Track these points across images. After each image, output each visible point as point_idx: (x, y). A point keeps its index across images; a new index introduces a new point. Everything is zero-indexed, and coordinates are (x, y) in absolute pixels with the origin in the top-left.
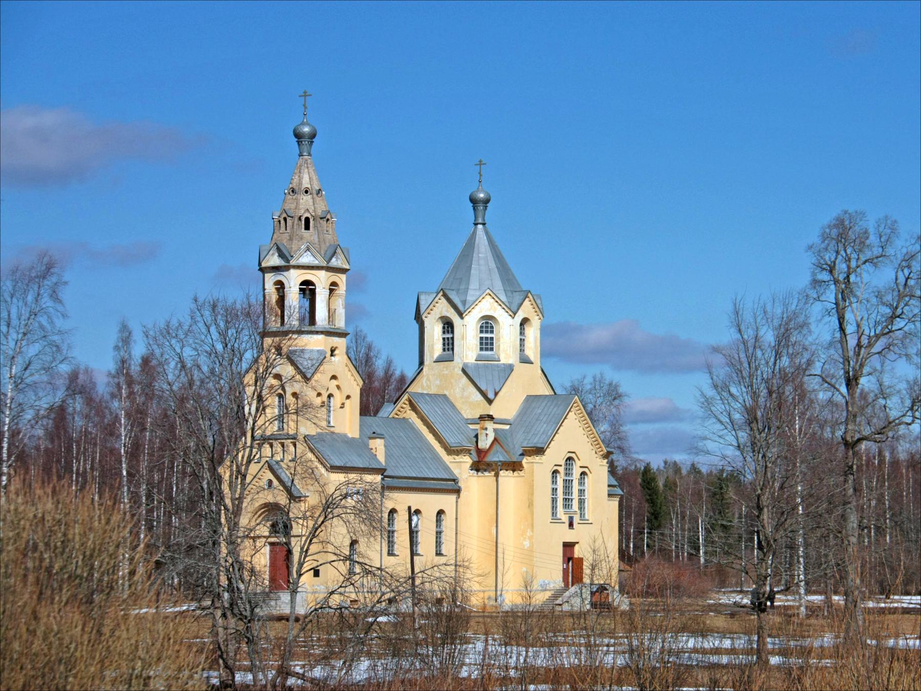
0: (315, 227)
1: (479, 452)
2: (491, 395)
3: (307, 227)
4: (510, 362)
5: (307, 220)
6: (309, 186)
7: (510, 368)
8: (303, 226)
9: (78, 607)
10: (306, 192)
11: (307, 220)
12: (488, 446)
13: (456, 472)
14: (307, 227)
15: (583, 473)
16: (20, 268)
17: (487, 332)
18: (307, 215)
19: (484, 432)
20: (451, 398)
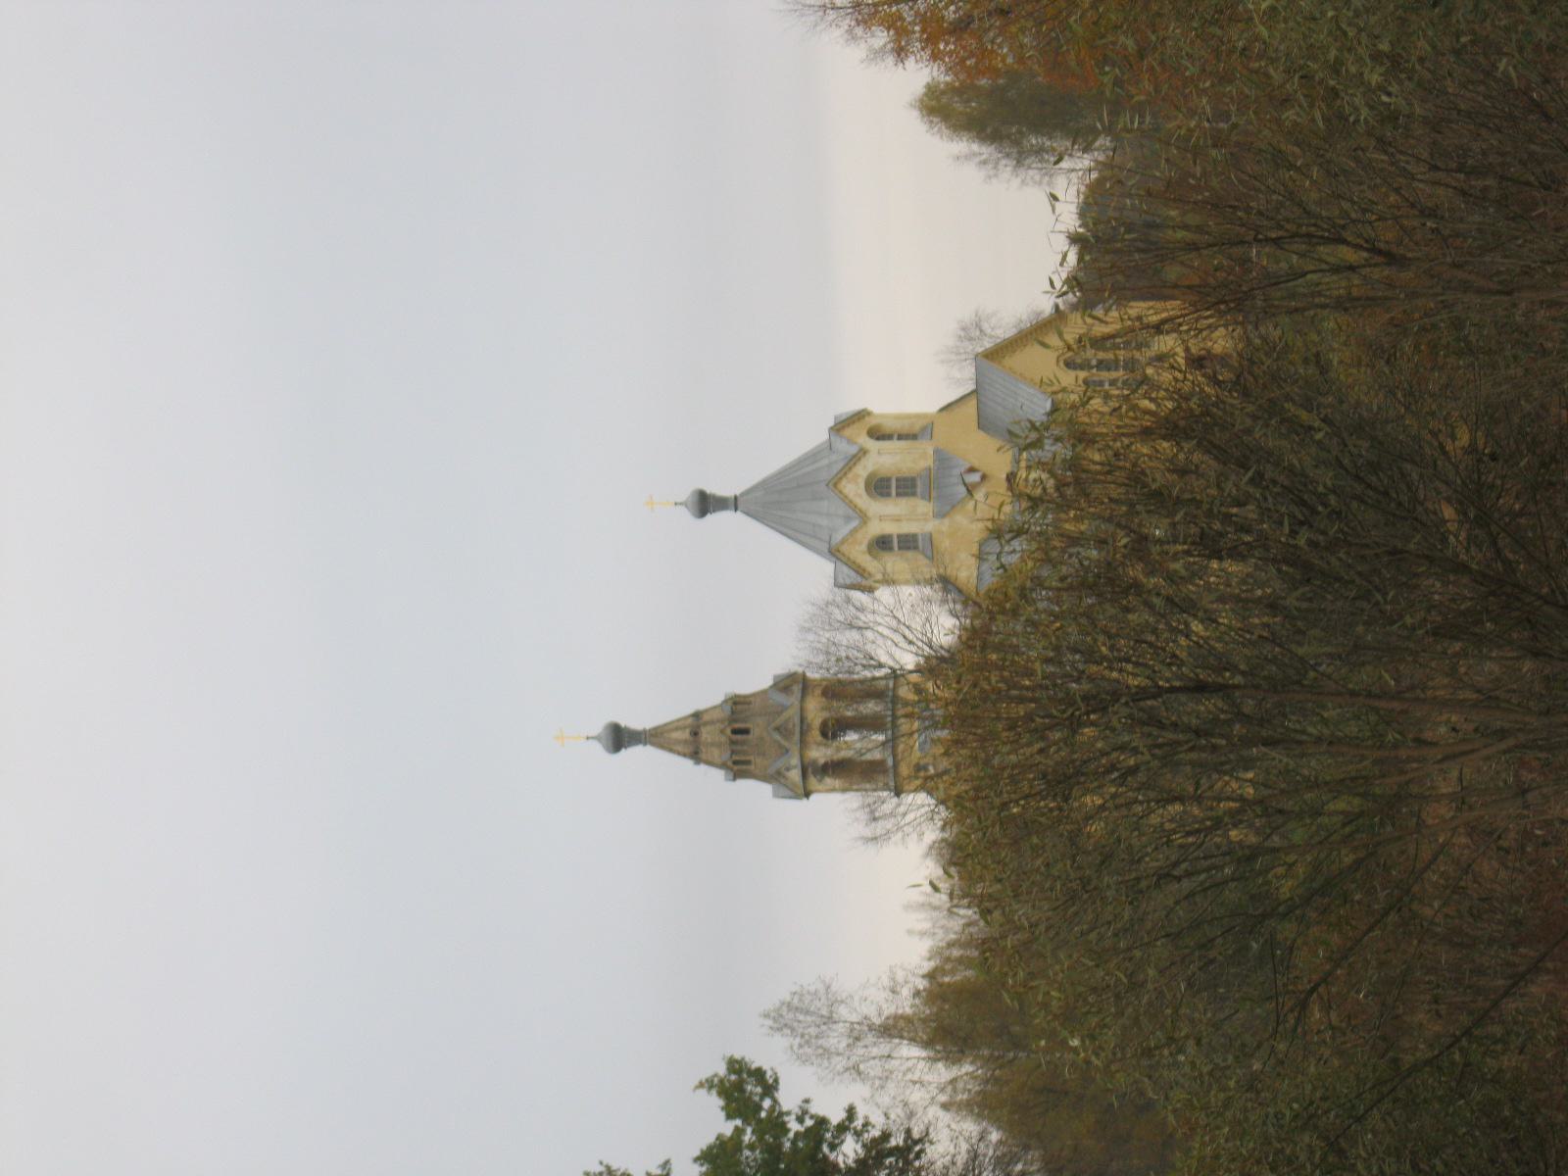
3: (746, 731)
4: (931, 452)
5: (735, 732)
7: (937, 452)
11: (735, 732)
14: (746, 731)
17: (889, 487)
18: (728, 731)
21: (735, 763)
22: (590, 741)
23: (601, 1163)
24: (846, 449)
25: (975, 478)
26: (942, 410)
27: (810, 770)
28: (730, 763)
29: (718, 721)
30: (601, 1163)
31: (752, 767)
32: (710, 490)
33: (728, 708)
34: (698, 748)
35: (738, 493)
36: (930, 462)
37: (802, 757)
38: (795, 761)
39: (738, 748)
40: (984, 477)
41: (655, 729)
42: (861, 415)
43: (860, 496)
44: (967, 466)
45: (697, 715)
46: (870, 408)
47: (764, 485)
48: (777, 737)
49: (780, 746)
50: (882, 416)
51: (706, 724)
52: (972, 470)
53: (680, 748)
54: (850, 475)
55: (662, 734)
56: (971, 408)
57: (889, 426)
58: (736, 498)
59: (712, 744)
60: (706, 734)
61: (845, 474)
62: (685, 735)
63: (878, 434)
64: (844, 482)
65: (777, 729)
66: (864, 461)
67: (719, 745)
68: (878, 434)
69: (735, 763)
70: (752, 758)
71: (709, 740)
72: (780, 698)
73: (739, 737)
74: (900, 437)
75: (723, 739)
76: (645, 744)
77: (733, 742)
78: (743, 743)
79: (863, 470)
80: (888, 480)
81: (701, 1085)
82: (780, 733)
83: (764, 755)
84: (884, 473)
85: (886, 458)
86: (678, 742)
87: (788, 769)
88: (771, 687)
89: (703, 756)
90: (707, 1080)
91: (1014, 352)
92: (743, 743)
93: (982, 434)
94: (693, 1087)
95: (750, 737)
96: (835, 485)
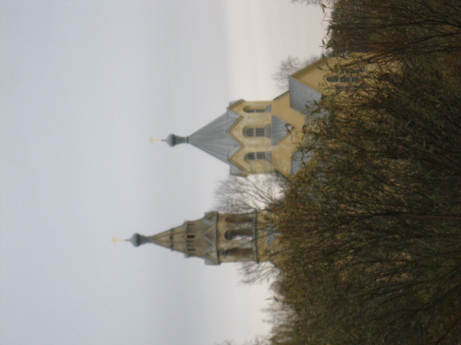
3: (193, 237)
4: (270, 117)
14: (193, 237)
18: (186, 237)
38: (214, 249)
40: (293, 128)
42: (240, 102)
45: (172, 230)
48: (206, 239)
51: (176, 234)
54: (236, 128)
56: (287, 99)
57: (253, 107)
60: (177, 238)
61: (234, 127)
62: (167, 238)
64: (234, 130)
65: (206, 235)
69: (189, 250)
73: (190, 239)
77: (188, 241)
79: (241, 125)
95: (195, 239)
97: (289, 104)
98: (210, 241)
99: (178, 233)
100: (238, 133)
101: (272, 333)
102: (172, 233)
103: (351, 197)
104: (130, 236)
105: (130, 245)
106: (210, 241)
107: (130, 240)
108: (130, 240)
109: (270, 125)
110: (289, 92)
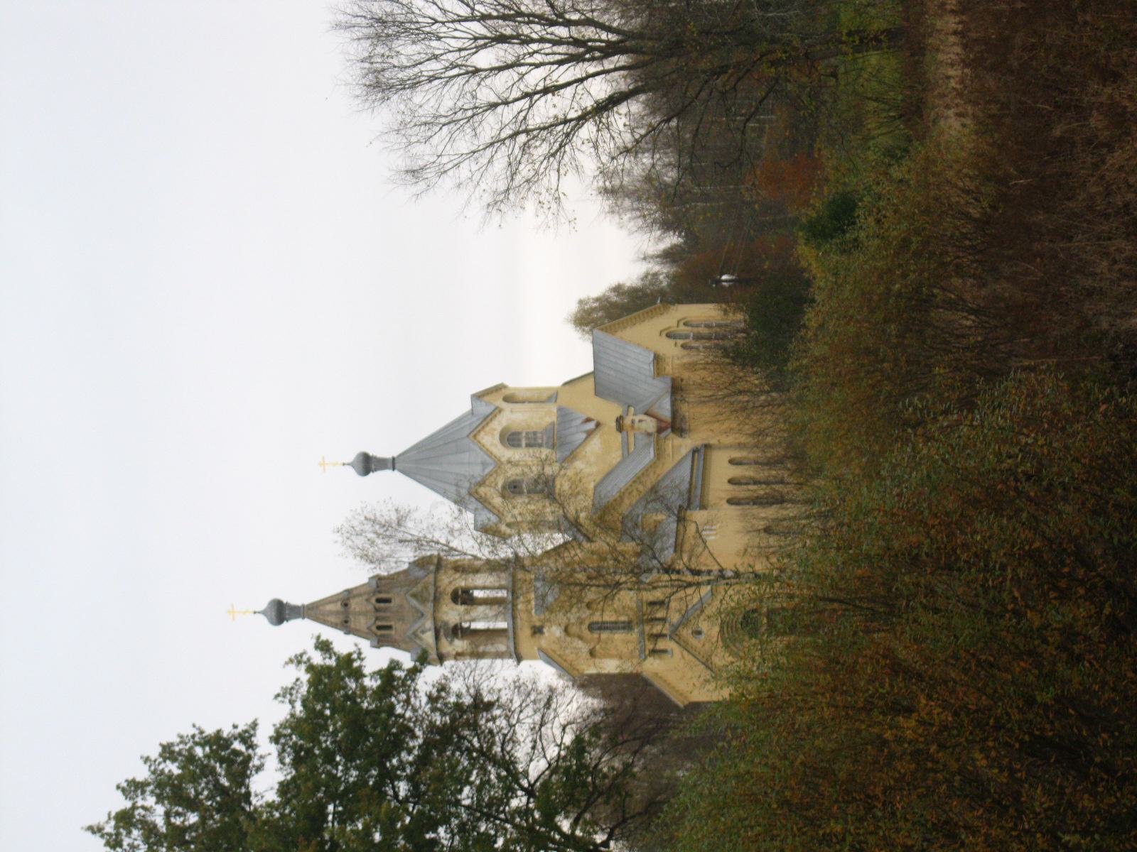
0: (388, 592)
1: (660, 430)
2: (591, 425)
3: (388, 601)
4: (555, 410)
5: (379, 601)
6: (339, 603)
7: (560, 409)
8: (387, 605)
9: (832, 578)
10: (346, 605)
11: (379, 601)
12: (654, 420)
13: (684, 451)
14: (388, 601)
15: (685, 324)
16: (400, 162)
17: (519, 440)
18: (373, 600)
19: (637, 424)
20: (598, 479)
21: (379, 628)
22: (257, 615)
23: (194, 726)
24: (484, 409)
25: (591, 425)
26: (566, 384)
27: (442, 633)
28: (374, 628)
29: (365, 593)
30: (194, 726)
31: (393, 632)
32: (371, 453)
33: (374, 583)
34: (347, 617)
35: (395, 455)
36: (554, 419)
37: (435, 619)
38: (429, 624)
39: (382, 614)
40: (598, 425)
41: (313, 604)
42: (499, 388)
43: (496, 446)
44: (585, 417)
45: (349, 591)
46: (506, 383)
47: (418, 447)
48: (414, 602)
49: (417, 611)
50: (515, 389)
51: (354, 597)
52: (588, 420)
53: (332, 619)
54: (487, 429)
55: (317, 607)
56: (590, 383)
57: (521, 396)
58: (394, 459)
59: (360, 613)
60: (355, 605)
61: (483, 428)
62: (338, 607)
63: (509, 399)
64: (482, 434)
65: (414, 596)
66: (499, 417)
67: (365, 614)
68: (509, 399)
69: (379, 628)
70: (392, 623)
71: (357, 610)
72: (419, 573)
73: (382, 605)
74: (530, 402)
75: (370, 607)
76: (304, 618)
77: (377, 610)
78: (385, 610)
79: (498, 425)
80: (519, 433)
81: (291, 661)
82: (417, 600)
83: (403, 620)
84: (515, 428)
85: (514, 417)
86: (331, 613)
87: (423, 632)
88: (429, 663)
89: (352, 625)
90: (296, 656)
91: (625, 328)
92: (385, 610)
93: (597, 400)
94: (283, 663)
95: (392, 605)
96: (475, 436)
97: (593, 392)
98: (420, 607)
99: (360, 595)
100: (490, 440)
101: (642, 279)
102: (346, 599)
103: (742, 115)
104: (351, 456)
105: (351, 472)
106: (420, 607)
107: (264, 613)
108: (264, 613)
109: (553, 424)
110: (593, 373)
